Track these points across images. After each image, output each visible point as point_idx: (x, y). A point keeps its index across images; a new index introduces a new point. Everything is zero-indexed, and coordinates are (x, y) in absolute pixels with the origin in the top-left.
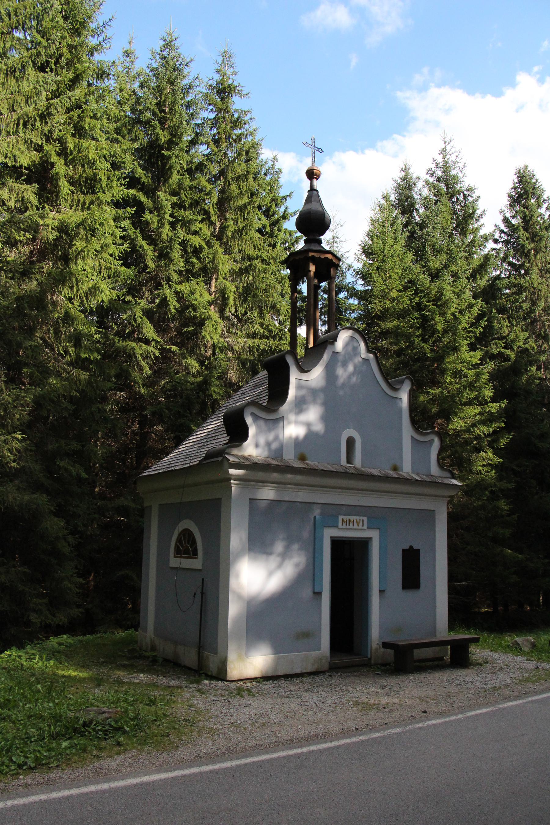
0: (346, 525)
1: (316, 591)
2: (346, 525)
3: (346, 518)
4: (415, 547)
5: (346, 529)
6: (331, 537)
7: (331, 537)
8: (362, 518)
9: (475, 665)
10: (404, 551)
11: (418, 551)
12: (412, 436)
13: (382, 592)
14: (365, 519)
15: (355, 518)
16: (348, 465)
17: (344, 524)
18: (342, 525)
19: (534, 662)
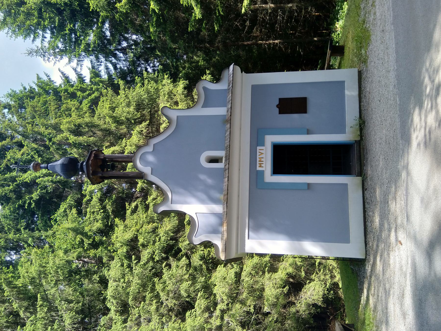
0: (263, 164)
1: (307, 189)
2: (263, 164)
3: (258, 165)
4: (277, 102)
5: (266, 154)
6: (271, 175)
7: (271, 175)
8: (258, 151)
9: (344, 44)
10: (280, 113)
11: (280, 99)
12: (202, 107)
13: (308, 132)
14: (258, 148)
15: (258, 157)
16: (224, 161)
17: (262, 165)
18: (263, 167)
19: (48, 123)
